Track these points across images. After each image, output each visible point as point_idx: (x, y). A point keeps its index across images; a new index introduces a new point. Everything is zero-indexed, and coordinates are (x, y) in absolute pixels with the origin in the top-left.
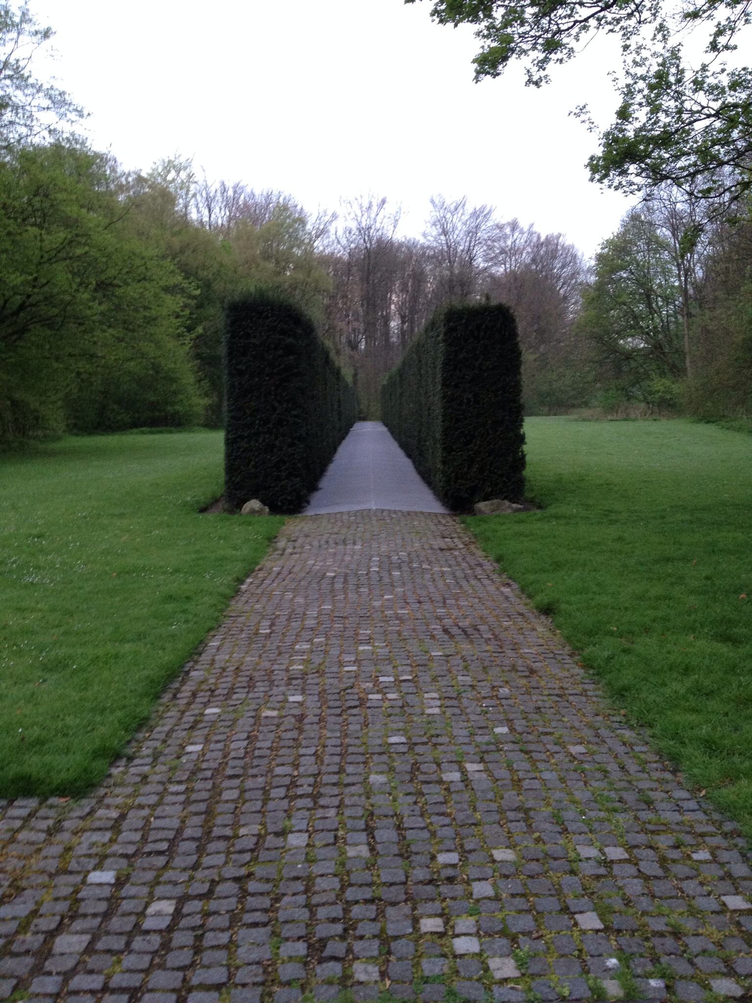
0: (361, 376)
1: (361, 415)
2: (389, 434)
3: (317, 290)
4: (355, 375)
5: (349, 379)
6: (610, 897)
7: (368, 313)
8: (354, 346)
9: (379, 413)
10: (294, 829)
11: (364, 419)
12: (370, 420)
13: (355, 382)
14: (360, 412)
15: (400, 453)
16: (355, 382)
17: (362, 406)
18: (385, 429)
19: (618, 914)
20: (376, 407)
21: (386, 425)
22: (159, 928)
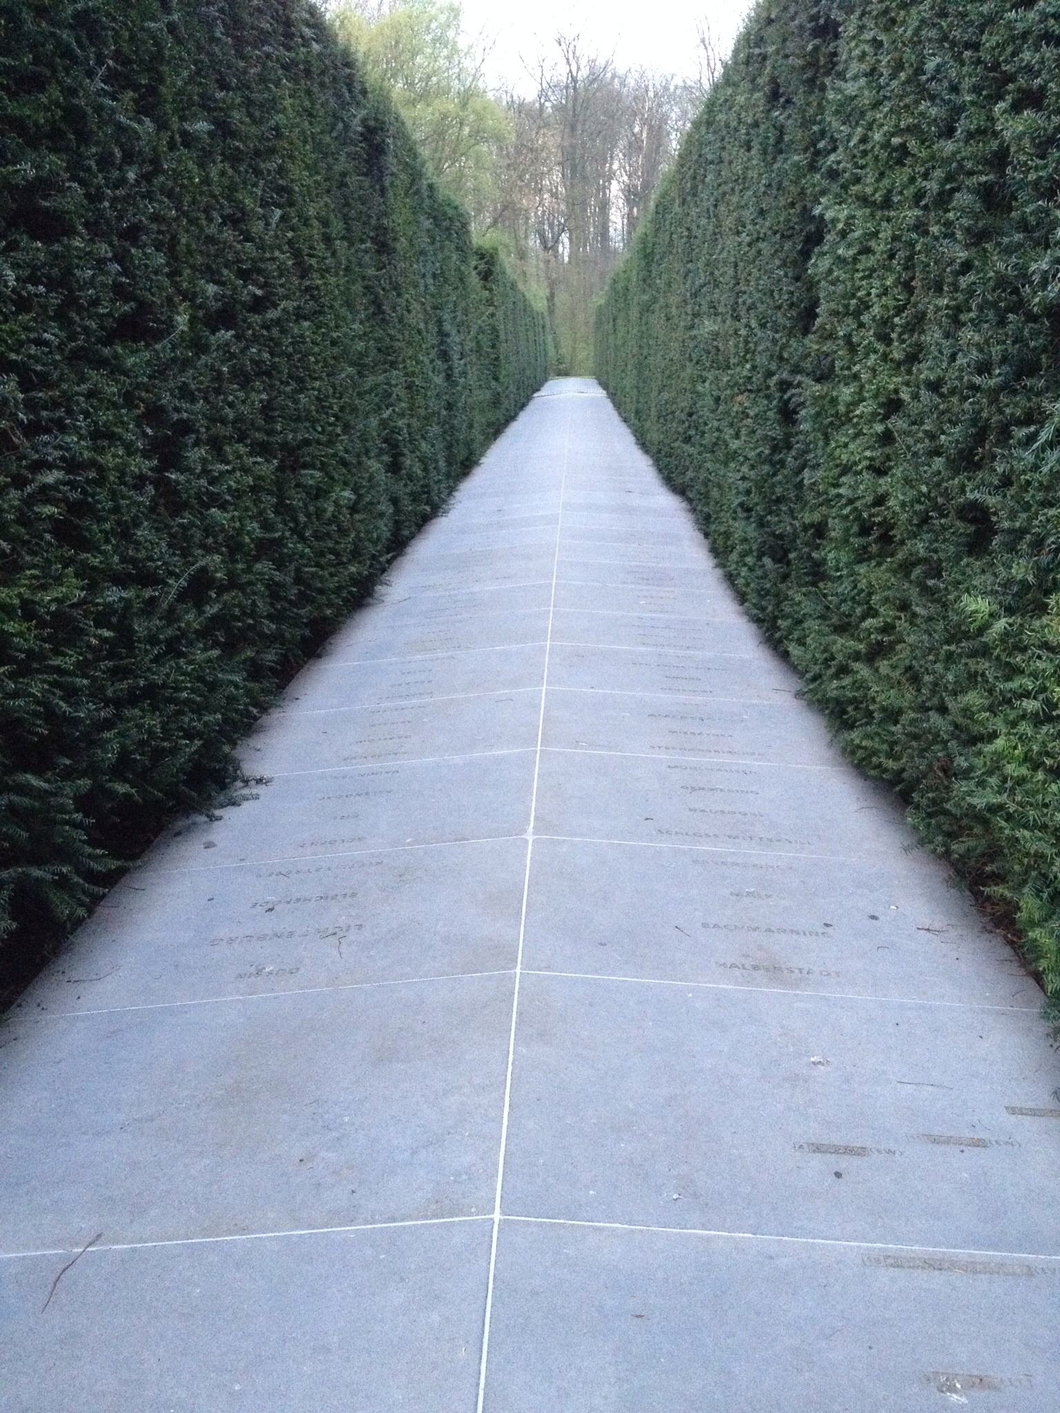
0: (562, 298)
1: (561, 367)
2: (609, 405)
3: (478, 134)
4: (551, 298)
5: (540, 305)
6: (996, 677)
7: (572, 185)
8: (549, 246)
9: (590, 364)
10: (914, 1087)
11: (566, 374)
12: (576, 375)
13: (551, 311)
14: (560, 362)
15: (642, 466)
16: (551, 311)
17: (563, 351)
18: (600, 393)
19: (777, 432)
20: (585, 353)
21: (605, 386)
22: (251, 802)
